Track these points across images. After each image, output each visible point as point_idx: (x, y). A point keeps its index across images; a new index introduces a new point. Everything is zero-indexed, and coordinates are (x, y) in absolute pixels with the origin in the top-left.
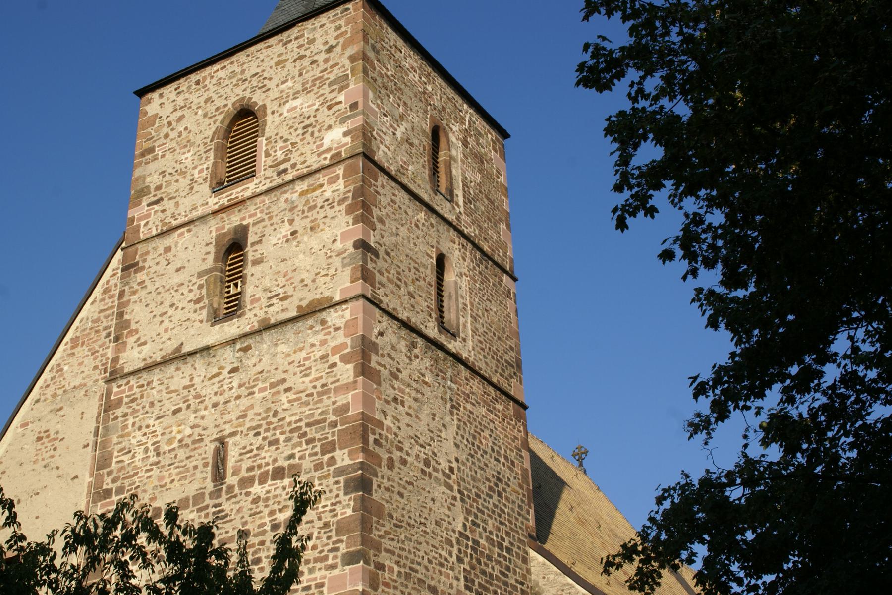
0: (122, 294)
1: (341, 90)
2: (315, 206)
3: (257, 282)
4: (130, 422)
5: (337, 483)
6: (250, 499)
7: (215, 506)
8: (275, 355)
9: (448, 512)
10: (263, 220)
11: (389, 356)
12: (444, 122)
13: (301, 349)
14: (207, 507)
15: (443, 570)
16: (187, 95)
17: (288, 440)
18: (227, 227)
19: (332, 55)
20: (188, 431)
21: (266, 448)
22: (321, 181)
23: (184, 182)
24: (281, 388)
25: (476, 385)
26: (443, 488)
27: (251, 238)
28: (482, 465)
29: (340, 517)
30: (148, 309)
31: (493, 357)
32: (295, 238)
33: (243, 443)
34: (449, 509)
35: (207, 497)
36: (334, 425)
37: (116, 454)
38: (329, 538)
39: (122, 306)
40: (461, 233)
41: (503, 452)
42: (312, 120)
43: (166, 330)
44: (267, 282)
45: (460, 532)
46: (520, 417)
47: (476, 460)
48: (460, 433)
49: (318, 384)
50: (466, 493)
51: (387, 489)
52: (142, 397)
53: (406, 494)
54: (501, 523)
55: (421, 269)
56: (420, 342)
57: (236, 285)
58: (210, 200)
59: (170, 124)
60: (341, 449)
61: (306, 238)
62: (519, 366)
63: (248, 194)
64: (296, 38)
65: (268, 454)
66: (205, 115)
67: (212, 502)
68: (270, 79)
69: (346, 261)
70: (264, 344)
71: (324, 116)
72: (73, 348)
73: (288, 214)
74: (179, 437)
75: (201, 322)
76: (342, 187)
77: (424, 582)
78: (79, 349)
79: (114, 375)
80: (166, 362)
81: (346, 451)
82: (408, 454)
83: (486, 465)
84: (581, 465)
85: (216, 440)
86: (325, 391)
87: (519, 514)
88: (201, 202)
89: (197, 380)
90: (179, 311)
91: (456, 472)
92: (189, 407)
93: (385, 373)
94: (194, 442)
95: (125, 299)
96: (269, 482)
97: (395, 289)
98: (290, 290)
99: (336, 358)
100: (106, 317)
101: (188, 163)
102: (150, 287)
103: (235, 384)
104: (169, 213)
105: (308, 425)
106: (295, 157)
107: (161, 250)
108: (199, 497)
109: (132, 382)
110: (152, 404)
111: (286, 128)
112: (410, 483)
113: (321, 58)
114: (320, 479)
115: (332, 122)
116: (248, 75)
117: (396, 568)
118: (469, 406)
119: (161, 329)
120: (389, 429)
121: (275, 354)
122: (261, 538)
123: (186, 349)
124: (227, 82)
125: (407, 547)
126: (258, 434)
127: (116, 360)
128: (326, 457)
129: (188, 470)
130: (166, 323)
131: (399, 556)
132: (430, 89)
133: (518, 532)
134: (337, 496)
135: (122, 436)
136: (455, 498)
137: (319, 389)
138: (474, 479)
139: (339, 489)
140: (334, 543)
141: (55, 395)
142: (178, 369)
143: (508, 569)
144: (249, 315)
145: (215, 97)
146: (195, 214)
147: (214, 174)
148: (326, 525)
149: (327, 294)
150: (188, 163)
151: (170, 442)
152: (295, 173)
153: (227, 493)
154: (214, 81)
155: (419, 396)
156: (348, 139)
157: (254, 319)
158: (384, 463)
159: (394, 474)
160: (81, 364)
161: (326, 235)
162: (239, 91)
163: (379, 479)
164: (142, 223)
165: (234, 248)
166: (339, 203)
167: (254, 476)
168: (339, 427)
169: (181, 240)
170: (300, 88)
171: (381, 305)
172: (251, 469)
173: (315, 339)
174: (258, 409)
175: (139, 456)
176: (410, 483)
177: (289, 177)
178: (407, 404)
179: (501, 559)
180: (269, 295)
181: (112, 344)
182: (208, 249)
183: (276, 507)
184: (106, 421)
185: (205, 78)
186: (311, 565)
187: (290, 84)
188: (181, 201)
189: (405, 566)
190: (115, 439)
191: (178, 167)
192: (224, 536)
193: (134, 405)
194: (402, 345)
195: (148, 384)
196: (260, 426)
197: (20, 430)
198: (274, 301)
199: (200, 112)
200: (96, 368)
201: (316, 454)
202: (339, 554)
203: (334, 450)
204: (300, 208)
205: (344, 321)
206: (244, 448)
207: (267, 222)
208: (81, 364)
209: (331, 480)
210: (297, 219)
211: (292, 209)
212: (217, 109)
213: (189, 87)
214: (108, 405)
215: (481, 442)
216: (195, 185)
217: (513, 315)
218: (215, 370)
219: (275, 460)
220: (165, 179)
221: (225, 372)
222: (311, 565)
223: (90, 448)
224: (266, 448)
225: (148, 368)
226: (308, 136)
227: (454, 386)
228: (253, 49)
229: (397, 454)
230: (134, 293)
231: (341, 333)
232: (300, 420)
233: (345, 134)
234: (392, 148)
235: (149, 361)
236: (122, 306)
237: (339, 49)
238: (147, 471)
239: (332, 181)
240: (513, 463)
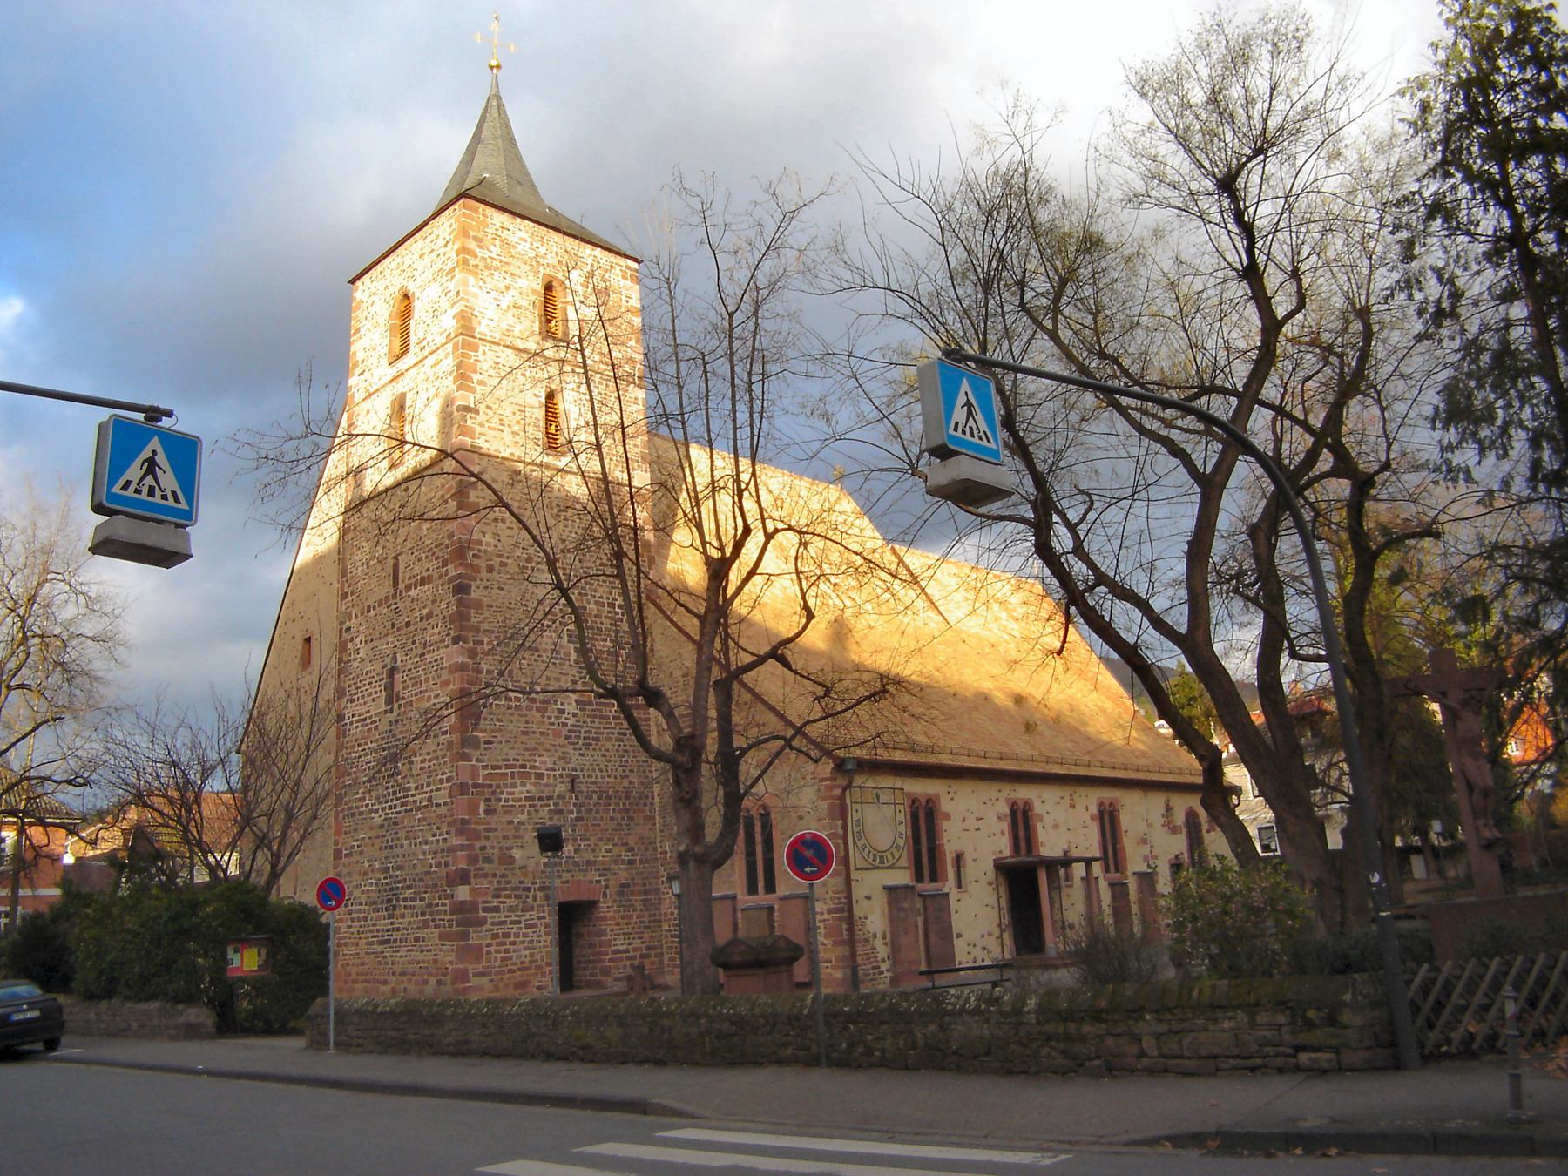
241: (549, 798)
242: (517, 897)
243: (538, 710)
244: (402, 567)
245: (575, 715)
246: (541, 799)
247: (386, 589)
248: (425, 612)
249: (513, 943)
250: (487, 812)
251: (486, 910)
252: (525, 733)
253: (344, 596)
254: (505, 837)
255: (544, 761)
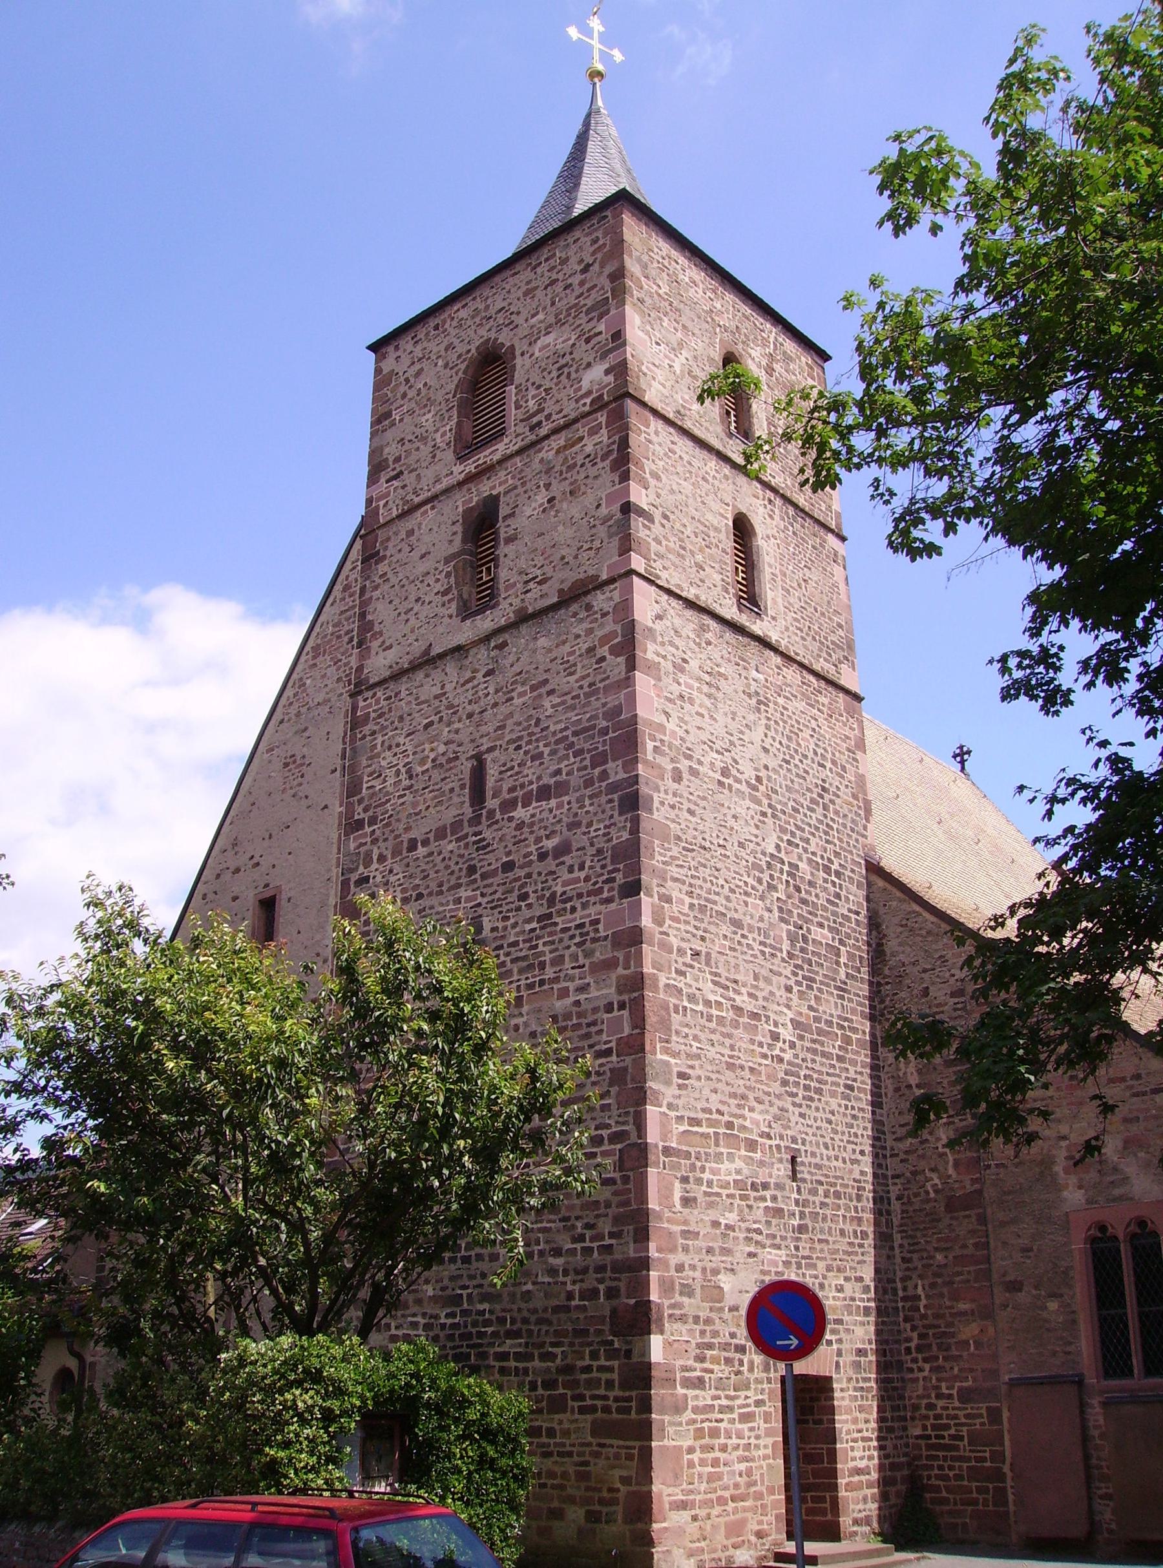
0: (363, 590)
1: (600, 317)
2: (575, 465)
3: (512, 563)
4: (379, 741)
5: (611, 801)
6: (513, 825)
7: (475, 834)
8: (535, 651)
9: (755, 831)
10: (515, 488)
11: (671, 643)
12: (740, 346)
13: (564, 642)
14: (466, 836)
15: (749, 900)
16: (425, 344)
17: (553, 753)
18: (475, 499)
19: (588, 275)
20: (442, 748)
21: (529, 763)
22: (580, 433)
23: (425, 450)
24: (543, 690)
25: (792, 674)
26: (748, 803)
27: (503, 511)
28: (801, 773)
29: (615, 842)
30: (392, 607)
31: (814, 639)
32: (553, 507)
33: (503, 759)
34: (757, 827)
35: (466, 824)
36: (604, 732)
37: (366, 779)
38: (603, 867)
39: (364, 604)
40: (766, 485)
41: (829, 756)
42: (568, 358)
43: (412, 631)
44: (522, 564)
45: (772, 855)
46: (851, 712)
47: (792, 767)
48: (771, 734)
49: (585, 683)
50: (779, 807)
51: (673, 807)
52: (390, 710)
53: (698, 811)
54: (827, 842)
55: (712, 534)
56: (713, 624)
57: (489, 569)
58: (454, 469)
59: (407, 380)
60: (614, 760)
61: (565, 505)
62: (850, 646)
63: (497, 457)
64: (547, 260)
65: (531, 772)
66: (446, 366)
67: (471, 830)
68: (518, 313)
69: (614, 529)
70: (519, 641)
71: (583, 352)
72: (314, 658)
73: (544, 477)
74: (432, 755)
75: (450, 617)
76: (605, 439)
77: (724, 915)
78: (321, 658)
79: (360, 687)
80: (414, 667)
81: (620, 762)
82: (700, 763)
83: (807, 772)
84: (963, 769)
85: (472, 757)
86: (593, 692)
87: (853, 830)
88: (445, 472)
89: (448, 687)
90: (426, 607)
91: (765, 782)
92: (441, 719)
93: (666, 666)
94: (449, 761)
95: (367, 596)
96: (534, 804)
97: (677, 561)
98: (549, 571)
99: (604, 651)
100: (347, 619)
101: (429, 426)
102: (394, 580)
103: (491, 690)
104: (409, 489)
105: (575, 734)
106: (550, 406)
107: (403, 535)
108: (457, 825)
109: (379, 694)
110: (401, 718)
111: (538, 371)
112: (704, 798)
113: (575, 280)
114: (590, 797)
115: (591, 359)
116: (492, 311)
117: (687, 900)
118: (781, 701)
119: (407, 630)
120: (673, 733)
121: (533, 650)
122: (527, 870)
123: (436, 651)
124: (469, 323)
125: (701, 875)
126: (519, 748)
127: (360, 669)
128: (597, 771)
129: (443, 794)
130: (413, 621)
131: (691, 885)
132: (719, 306)
133: (851, 853)
134: (612, 817)
135: (370, 758)
136: (764, 814)
137: (587, 690)
138: (789, 789)
139: (612, 809)
140: (609, 872)
141: (298, 714)
142: (427, 676)
143: (838, 896)
144: (504, 605)
145: (456, 342)
146: (439, 487)
147: (458, 436)
148: (600, 851)
149: (591, 572)
150: (429, 426)
151: (423, 761)
152: (551, 426)
153: (488, 818)
154: (455, 323)
155: (713, 691)
156: (611, 378)
157: (510, 610)
158: (668, 775)
159: (681, 788)
160: (324, 676)
161: (589, 500)
162: (483, 332)
163: (662, 795)
164: (382, 503)
165: (483, 526)
166: (603, 460)
167: (516, 798)
168: (611, 735)
169: (426, 519)
170: (553, 320)
171: (658, 582)
172: (512, 790)
173: (579, 629)
174: (517, 717)
175: (391, 781)
176: (704, 798)
177: (543, 432)
178: (698, 701)
179: (829, 885)
180: (526, 578)
181: (356, 651)
182: (455, 528)
183: (542, 833)
184: (353, 740)
185: (444, 322)
186: (584, 900)
187: (541, 316)
188: (423, 472)
189: (699, 897)
190: (365, 763)
191: (418, 431)
192: (487, 868)
193: (381, 720)
194: (689, 630)
195: (396, 695)
196: (520, 738)
197: (266, 756)
198: (532, 585)
199: (440, 363)
200: (339, 680)
201: (585, 768)
202: (616, 885)
203: (605, 762)
204: (557, 468)
205: (612, 603)
206: (504, 765)
207: (520, 490)
208: (324, 676)
209: (604, 799)
210: (554, 483)
211: (548, 471)
212: (459, 356)
213: (427, 334)
214: (356, 723)
215: (799, 745)
216: (438, 452)
217: (842, 586)
218: (468, 674)
219: (539, 778)
220: (405, 448)
221: (480, 675)
222: (584, 900)
223: (338, 773)
224: (529, 763)
225: (396, 676)
226: (563, 377)
227: (761, 677)
228: (497, 279)
229: (684, 765)
230: (376, 588)
231: (610, 618)
232: (566, 728)
233: (607, 372)
234: (668, 384)
235: (396, 668)
236: (364, 604)
237: (596, 266)
238: (400, 797)
239: (593, 432)
240: (844, 768)
241: (765, 1186)
242: (728, 1361)
243: (746, 1027)
244: (492, 773)
245: (792, 1045)
246: (754, 1186)
247: (460, 806)
248: (549, 844)
249: (724, 1448)
250: (687, 1201)
251: (688, 1383)
252: (731, 1066)
253: (353, 826)
254: (709, 1251)
255: (756, 1119)
